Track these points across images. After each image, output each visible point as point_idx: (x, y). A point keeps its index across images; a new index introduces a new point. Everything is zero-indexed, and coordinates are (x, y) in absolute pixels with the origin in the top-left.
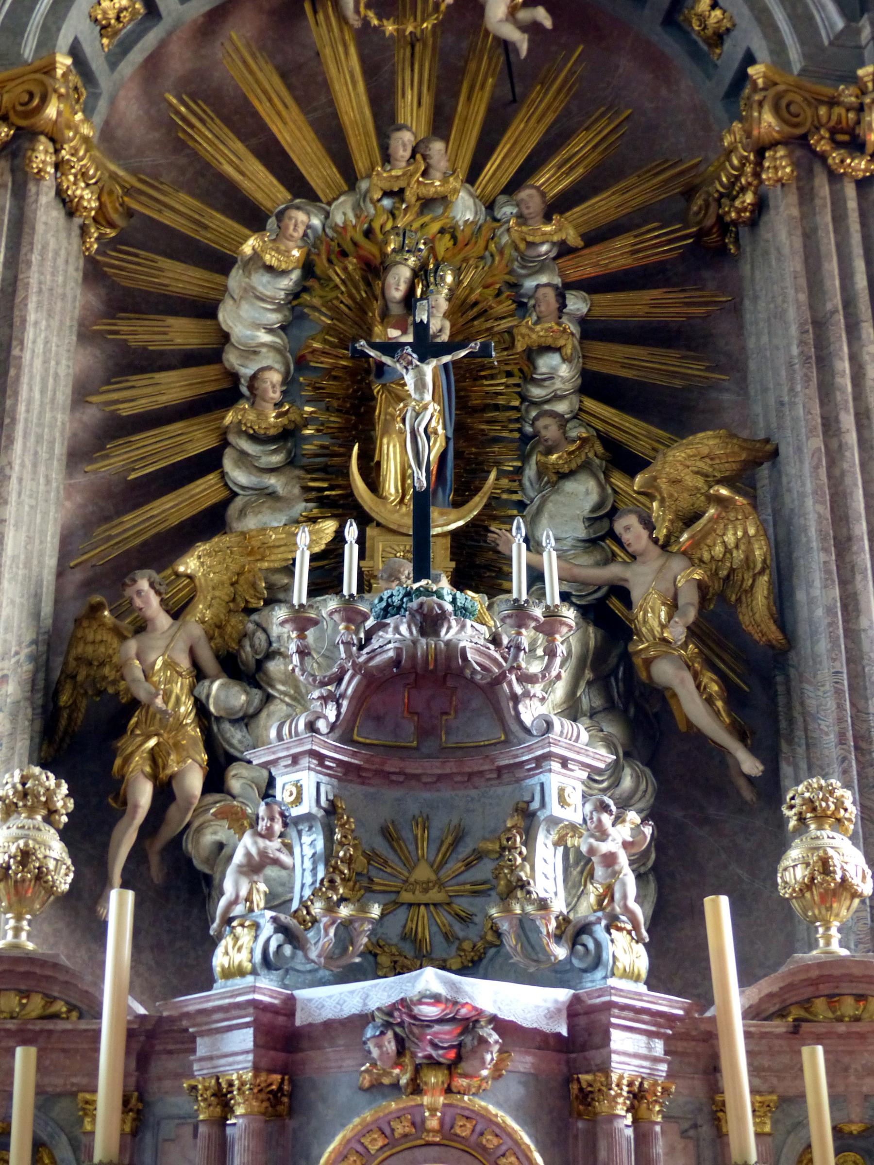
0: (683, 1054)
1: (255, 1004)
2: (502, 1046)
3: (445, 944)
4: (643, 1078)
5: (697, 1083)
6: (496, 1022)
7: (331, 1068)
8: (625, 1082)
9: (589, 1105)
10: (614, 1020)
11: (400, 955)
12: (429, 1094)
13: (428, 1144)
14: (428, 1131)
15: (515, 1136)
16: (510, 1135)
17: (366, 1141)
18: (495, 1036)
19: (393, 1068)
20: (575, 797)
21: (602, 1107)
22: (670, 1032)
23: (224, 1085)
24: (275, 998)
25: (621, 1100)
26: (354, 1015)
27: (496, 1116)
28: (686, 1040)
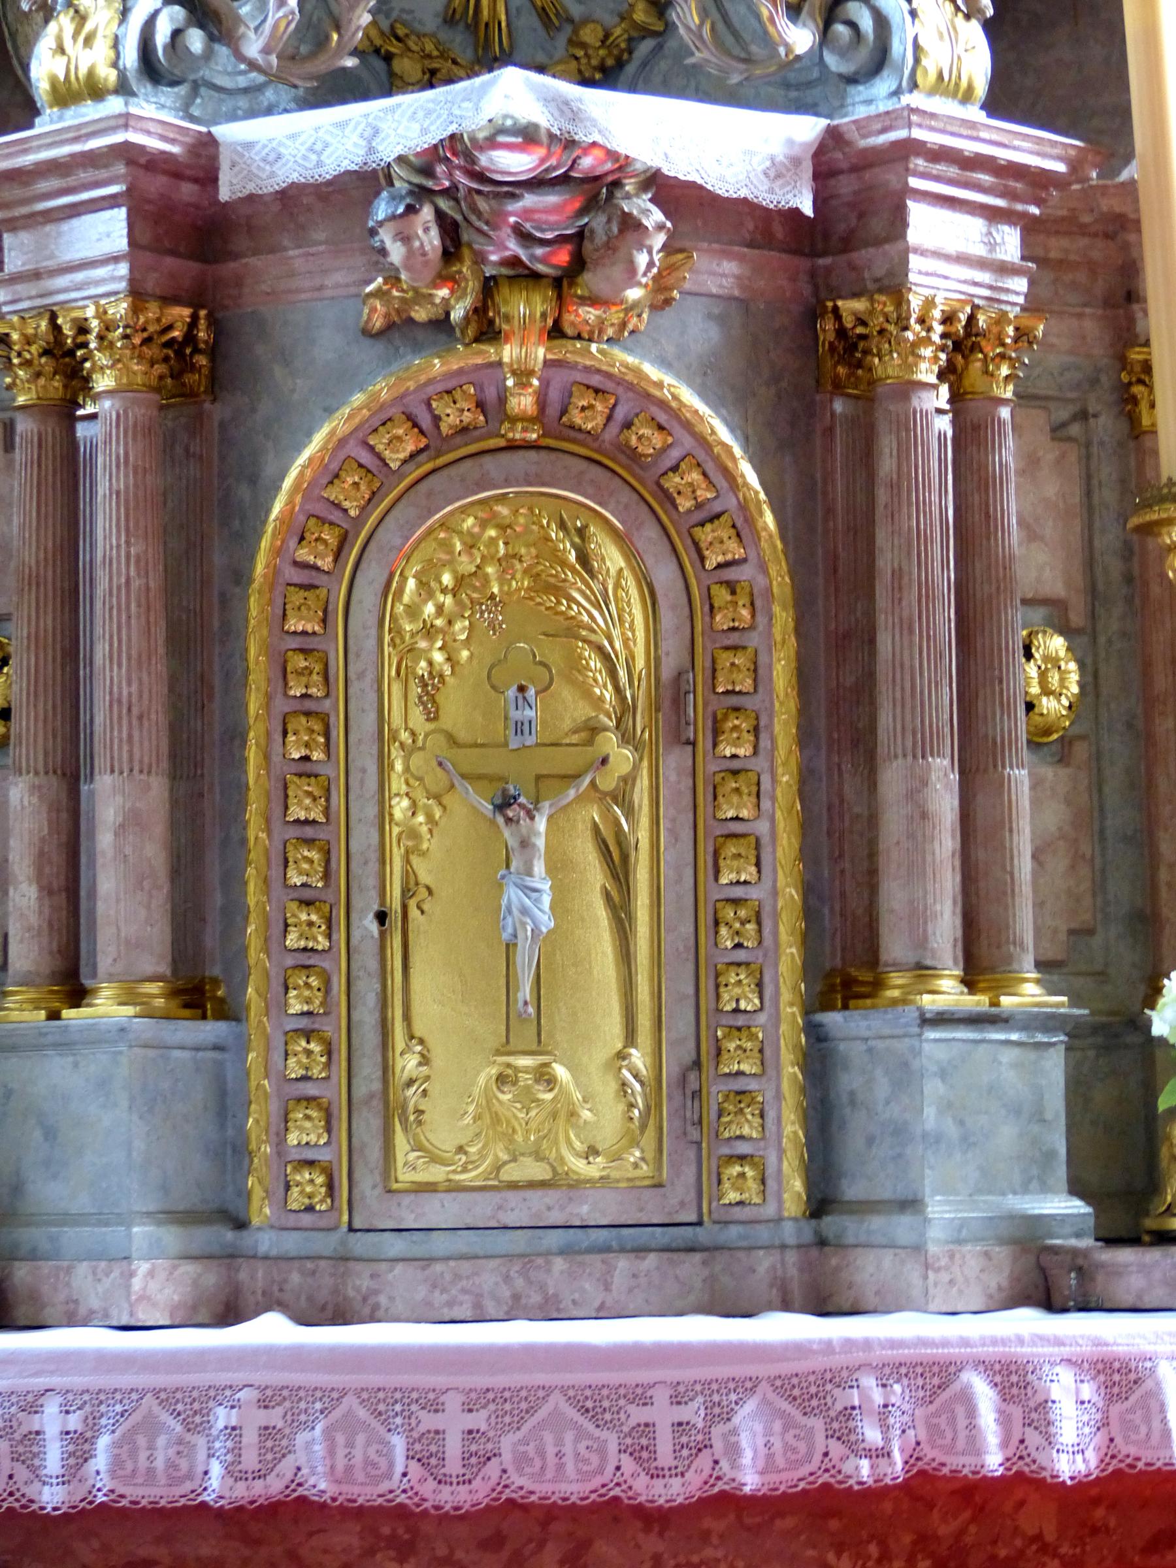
0: (1061, 265)
1: (127, 153)
2: (671, 236)
3: (541, 31)
4: (975, 307)
5: (1091, 327)
7: (298, 291)
8: (937, 314)
9: (860, 365)
10: (914, 182)
11: (443, 55)
12: (515, 340)
13: (513, 447)
14: (513, 420)
15: (699, 428)
17: (379, 442)
18: (656, 216)
19: (436, 286)
21: (887, 367)
22: (1035, 210)
23: (68, 331)
24: (172, 141)
25: (927, 352)
26: (348, 173)
27: (660, 385)
28: (1068, 233)
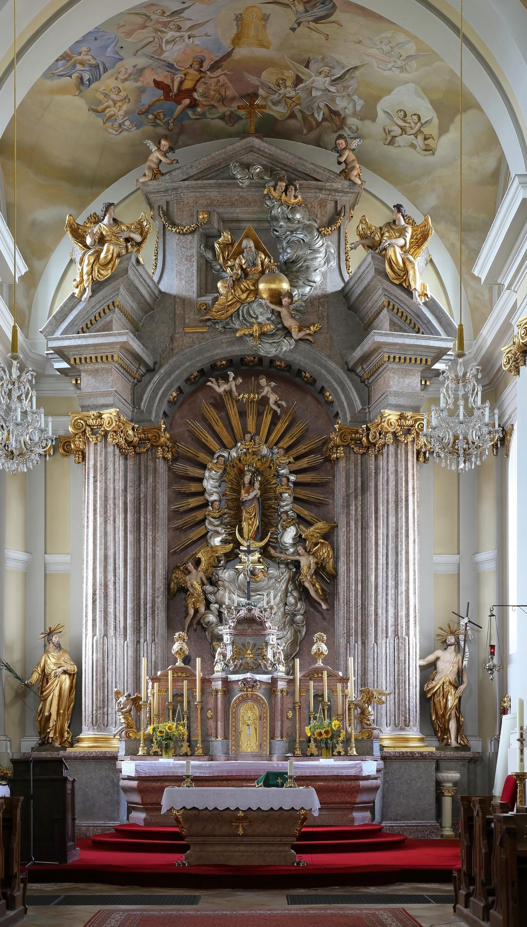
6: (260, 681)
16: (262, 698)
20: (275, 640)
